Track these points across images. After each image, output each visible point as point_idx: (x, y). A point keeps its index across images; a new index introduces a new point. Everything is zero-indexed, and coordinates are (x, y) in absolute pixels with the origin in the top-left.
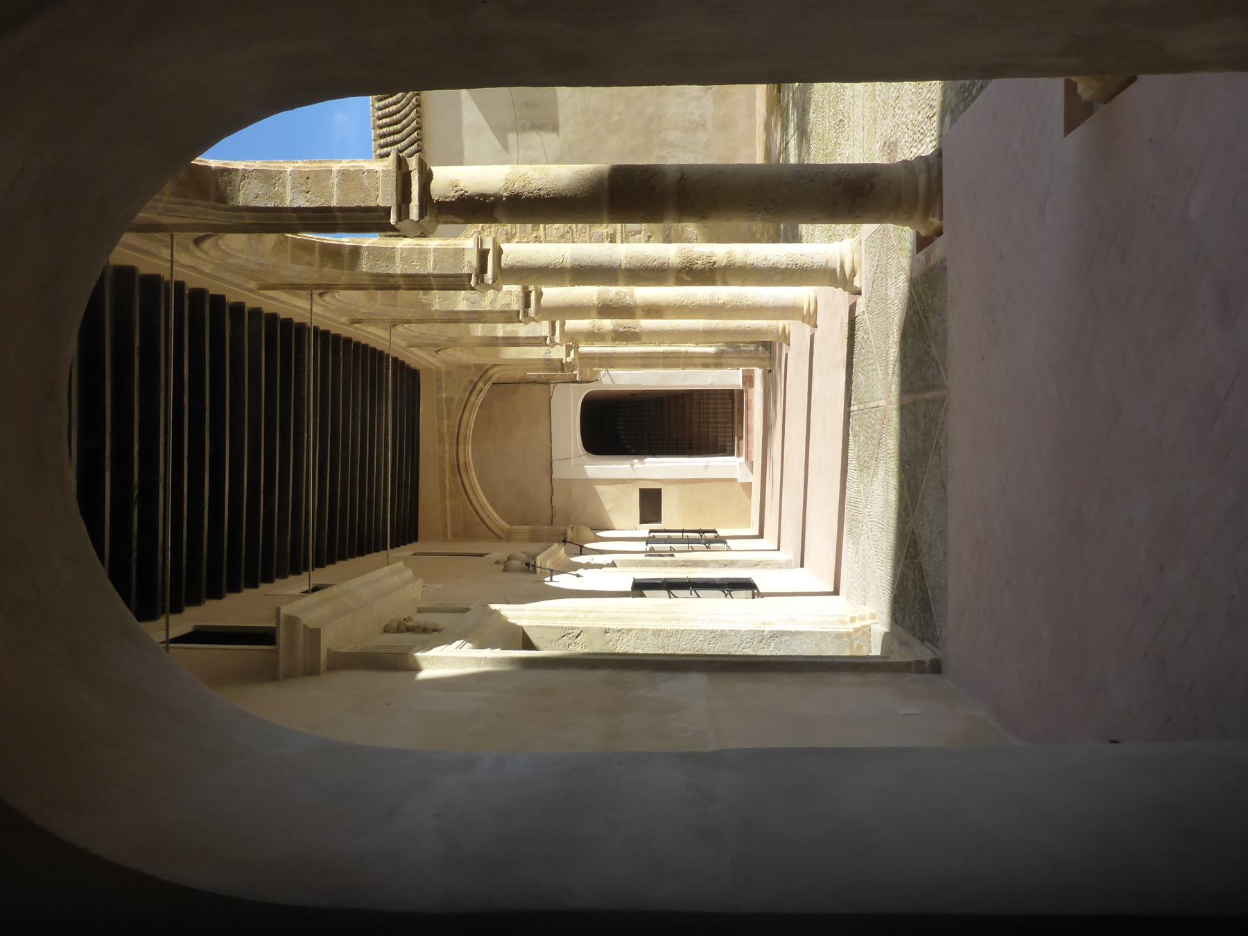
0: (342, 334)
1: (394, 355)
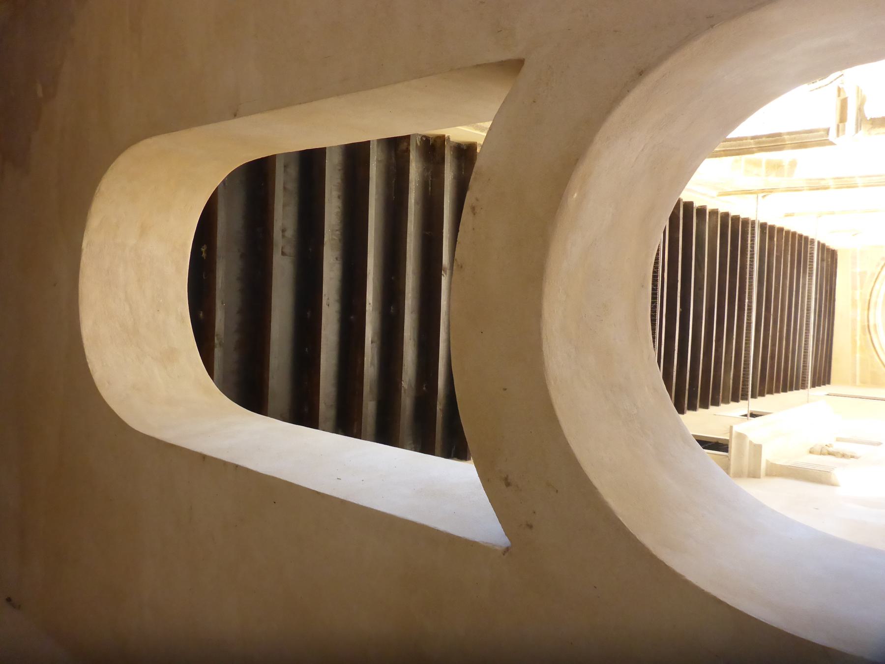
0: (776, 225)
1: (762, 221)
